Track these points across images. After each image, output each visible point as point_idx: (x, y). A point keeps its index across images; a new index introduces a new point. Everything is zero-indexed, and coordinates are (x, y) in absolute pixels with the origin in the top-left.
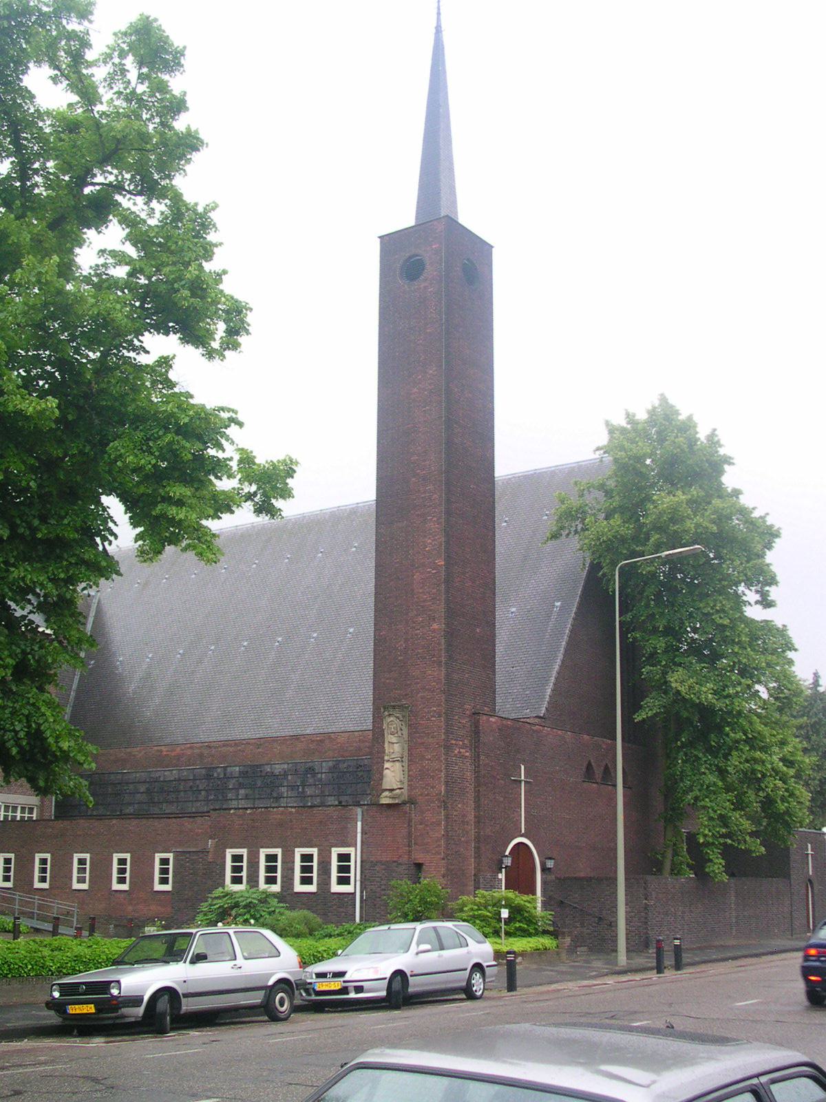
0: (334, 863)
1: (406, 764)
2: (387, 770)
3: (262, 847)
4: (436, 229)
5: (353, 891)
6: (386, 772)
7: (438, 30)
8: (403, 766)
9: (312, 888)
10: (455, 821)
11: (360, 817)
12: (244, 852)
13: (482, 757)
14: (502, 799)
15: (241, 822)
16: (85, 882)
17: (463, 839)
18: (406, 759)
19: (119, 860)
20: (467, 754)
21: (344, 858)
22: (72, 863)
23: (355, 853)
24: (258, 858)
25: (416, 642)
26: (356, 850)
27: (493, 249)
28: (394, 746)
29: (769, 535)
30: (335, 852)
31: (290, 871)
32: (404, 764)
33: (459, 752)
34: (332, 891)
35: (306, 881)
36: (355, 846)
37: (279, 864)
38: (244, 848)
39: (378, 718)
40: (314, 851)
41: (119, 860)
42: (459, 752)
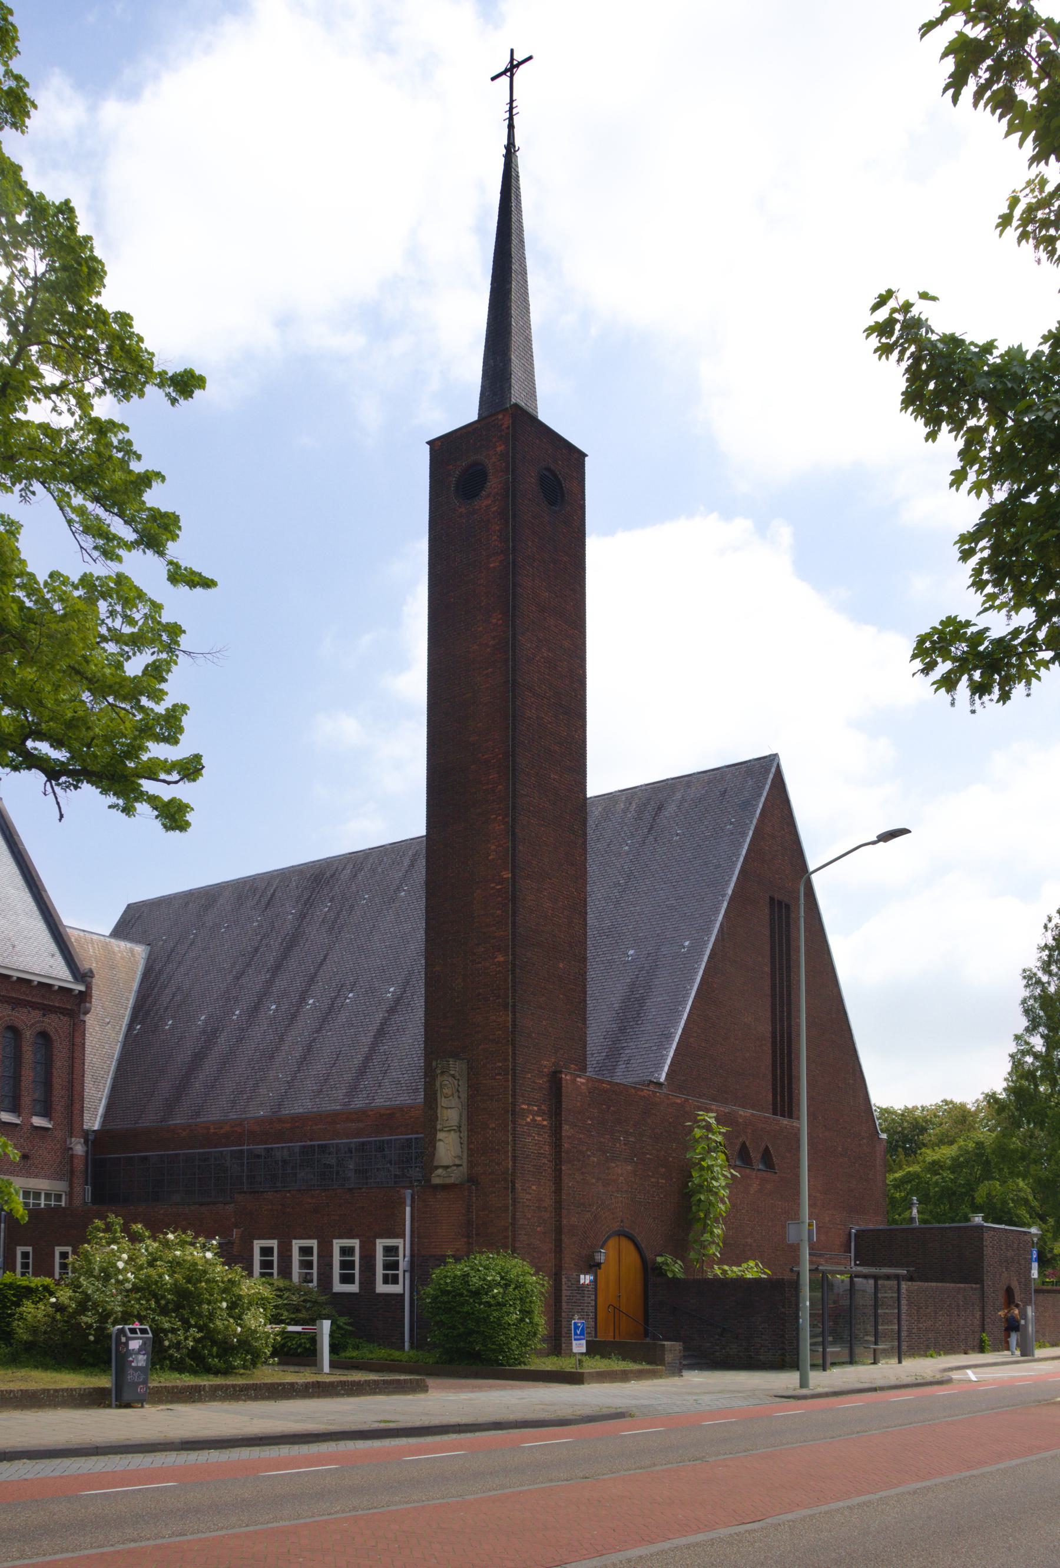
0: (337, 1258)
1: (465, 1134)
2: (441, 1143)
3: (295, 1239)
4: (502, 424)
5: (402, 1292)
6: (440, 1145)
7: (510, 150)
8: (461, 1138)
9: (354, 1288)
10: (528, 1206)
11: (408, 1202)
12: (274, 1243)
13: (565, 1127)
14: (594, 1181)
15: (270, 1207)
16: (353, 1283)
17: (539, 1229)
18: (464, 1128)
19: (23, 1253)
20: (545, 1123)
21: (390, 1251)
22: (53, 1257)
23: (403, 1245)
24: (290, 1250)
25: (477, 979)
26: (405, 1241)
27: (586, 458)
28: (451, 1112)
29: (907, 301)
30: (380, 1244)
31: (327, 1268)
32: (462, 1135)
33: (534, 1120)
34: (334, 1291)
35: (347, 1279)
36: (403, 1236)
37: (315, 1258)
38: (274, 1238)
39: (430, 1075)
40: (355, 1243)
41: (23, 1253)
42: (534, 1120)
